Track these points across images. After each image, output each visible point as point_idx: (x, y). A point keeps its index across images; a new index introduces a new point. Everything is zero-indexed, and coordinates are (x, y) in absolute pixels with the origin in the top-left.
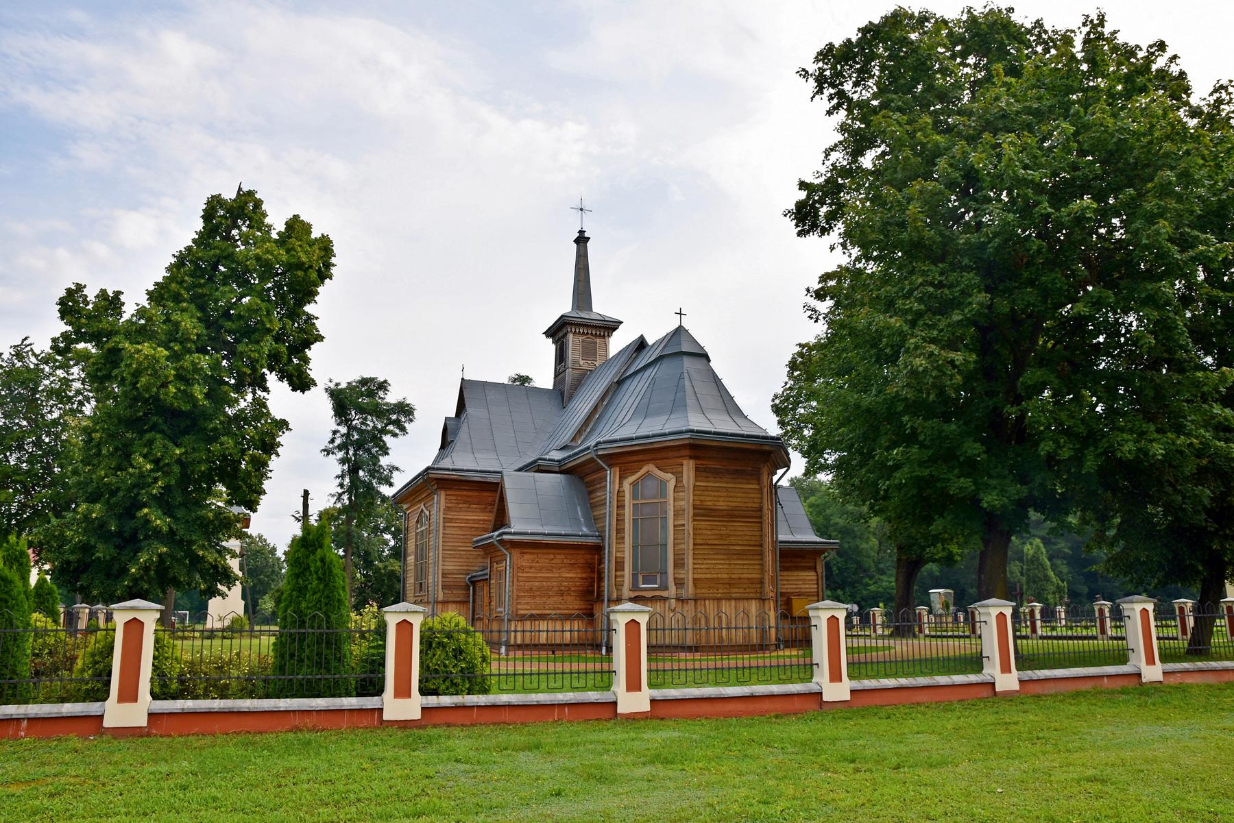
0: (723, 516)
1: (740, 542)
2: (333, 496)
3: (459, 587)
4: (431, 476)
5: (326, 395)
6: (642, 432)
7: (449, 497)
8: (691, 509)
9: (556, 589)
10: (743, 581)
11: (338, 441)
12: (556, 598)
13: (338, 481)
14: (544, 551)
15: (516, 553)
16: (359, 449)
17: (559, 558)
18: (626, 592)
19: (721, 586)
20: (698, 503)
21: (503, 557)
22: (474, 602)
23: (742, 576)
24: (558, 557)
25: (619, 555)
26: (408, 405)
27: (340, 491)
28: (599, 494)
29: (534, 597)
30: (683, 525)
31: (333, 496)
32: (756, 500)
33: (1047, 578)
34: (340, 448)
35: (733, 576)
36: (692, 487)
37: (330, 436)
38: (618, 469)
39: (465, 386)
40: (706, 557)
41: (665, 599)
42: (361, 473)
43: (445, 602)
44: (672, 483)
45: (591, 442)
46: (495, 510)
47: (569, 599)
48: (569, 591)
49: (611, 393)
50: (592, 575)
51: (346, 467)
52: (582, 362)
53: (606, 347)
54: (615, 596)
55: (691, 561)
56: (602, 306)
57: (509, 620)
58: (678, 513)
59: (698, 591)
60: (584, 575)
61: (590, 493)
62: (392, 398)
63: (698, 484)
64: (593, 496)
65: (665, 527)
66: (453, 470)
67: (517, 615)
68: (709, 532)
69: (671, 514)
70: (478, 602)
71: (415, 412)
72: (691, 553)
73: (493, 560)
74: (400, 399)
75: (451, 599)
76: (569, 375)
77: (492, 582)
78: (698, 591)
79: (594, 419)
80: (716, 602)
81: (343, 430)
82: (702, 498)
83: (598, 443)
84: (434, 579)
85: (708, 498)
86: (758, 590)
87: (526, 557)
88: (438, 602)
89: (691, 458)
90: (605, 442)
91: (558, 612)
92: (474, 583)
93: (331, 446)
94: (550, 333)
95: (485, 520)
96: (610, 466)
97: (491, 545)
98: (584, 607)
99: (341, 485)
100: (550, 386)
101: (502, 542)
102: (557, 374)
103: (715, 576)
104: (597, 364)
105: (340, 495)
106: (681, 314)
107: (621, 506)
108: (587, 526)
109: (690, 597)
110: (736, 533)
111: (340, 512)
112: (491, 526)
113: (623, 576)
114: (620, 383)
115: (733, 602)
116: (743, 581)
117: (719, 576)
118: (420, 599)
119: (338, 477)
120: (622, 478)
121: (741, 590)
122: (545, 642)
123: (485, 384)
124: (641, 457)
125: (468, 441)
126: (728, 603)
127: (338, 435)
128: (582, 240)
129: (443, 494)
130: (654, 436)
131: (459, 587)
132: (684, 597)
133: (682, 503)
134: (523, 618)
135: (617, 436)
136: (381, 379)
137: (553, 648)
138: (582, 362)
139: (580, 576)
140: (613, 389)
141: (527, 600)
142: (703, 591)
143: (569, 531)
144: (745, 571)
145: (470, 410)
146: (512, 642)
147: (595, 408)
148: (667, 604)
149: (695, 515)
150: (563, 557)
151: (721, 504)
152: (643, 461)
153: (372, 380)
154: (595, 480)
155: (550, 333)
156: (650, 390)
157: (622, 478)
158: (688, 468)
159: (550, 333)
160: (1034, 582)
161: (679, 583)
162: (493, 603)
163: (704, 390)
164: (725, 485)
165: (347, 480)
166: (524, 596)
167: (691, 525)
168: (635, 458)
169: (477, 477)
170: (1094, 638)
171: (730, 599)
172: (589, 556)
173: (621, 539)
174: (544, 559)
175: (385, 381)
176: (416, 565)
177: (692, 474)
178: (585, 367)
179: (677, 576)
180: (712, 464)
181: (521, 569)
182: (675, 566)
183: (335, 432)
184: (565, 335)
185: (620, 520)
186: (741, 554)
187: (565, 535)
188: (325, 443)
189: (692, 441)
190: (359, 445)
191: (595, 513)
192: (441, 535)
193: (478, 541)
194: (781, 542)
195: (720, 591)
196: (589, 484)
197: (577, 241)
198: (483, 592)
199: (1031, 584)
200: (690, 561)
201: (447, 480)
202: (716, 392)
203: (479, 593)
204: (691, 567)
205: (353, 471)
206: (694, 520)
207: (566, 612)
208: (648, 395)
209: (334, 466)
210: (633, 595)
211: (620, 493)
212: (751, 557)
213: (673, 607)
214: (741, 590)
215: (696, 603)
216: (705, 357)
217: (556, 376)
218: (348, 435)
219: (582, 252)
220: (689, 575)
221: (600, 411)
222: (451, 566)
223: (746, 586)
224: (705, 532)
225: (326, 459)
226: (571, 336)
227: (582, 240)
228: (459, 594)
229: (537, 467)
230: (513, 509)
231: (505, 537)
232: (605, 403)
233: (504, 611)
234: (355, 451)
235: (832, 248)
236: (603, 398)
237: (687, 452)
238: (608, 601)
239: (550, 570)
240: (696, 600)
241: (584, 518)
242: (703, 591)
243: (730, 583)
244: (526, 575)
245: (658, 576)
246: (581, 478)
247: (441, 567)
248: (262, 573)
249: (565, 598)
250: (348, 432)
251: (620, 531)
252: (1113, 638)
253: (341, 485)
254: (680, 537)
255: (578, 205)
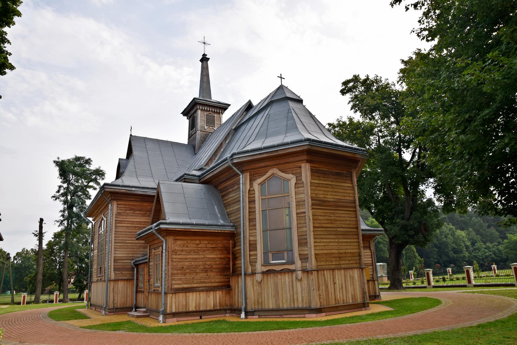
0: (331, 206)
1: (344, 226)
2: (58, 222)
3: (127, 269)
4: (106, 190)
5: (54, 164)
6: (265, 145)
7: (119, 206)
8: (310, 200)
9: (202, 267)
10: (348, 255)
11: (62, 191)
12: (202, 275)
13: (61, 214)
14: (193, 238)
15: (170, 239)
16: (73, 196)
17: (204, 243)
18: (259, 268)
19: (333, 259)
20: (314, 195)
21: (160, 244)
22: (137, 279)
23: (347, 251)
24: (202, 242)
25: (252, 238)
26: (101, 171)
27: (62, 218)
28: (231, 195)
29: (185, 274)
30: (304, 213)
31: (58, 222)
32: (351, 195)
33: (415, 257)
34: (63, 195)
35: (341, 251)
36: (309, 183)
37: (57, 189)
38: (248, 174)
39: (132, 139)
40: (323, 237)
41: (292, 271)
42: (74, 209)
43: (116, 280)
44: (293, 181)
45: (228, 155)
46: (152, 215)
47: (212, 274)
48: (211, 269)
49: (230, 136)
50: (228, 256)
51: (66, 206)
52: (206, 127)
53: (220, 119)
54: (250, 271)
55: (312, 240)
56: (216, 96)
57: (166, 293)
58: (300, 204)
59: (319, 264)
60: (222, 256)
61: (223, 196)
62: (93, 167)
63: (313, 181)
64: (226, 198)
65: (289, 215)
66: (123, 186)
67: (172, 289)
68: (323, 218)
69: (294, 204)
70: (140, 278)
71: (106, 175)
72: (312, 234)
73: (152, 247)
74: (97, 167)
75: (121, 278)
76: (199, 135)
77: (151, 264)
78: (319, 264)
79: (220, 152)
80: (331, 271)
81: (65, 185)
82: (317, 192)
83: (234, 154)
84: (110, 265)
85: (320, 192)
86: (358, 262)
87: (178, 242)
88: (110, 280)
89: (308, 161)
90: (239, 153)
91: (204, 285)
92: (137, 266)
93: (58, 194)
94: (185, 112)
95: (145, 222)
96: (243, 172)
97: (152, 234)
98: (223, 280)
99: (63, 216)
100: (186, 142)
101: (160, 231)
102: (190, 137)
103: (329, 251)
104: (215, 129)
105: (62, 221)
106: (281, 78)
107: (252, 201)
108: (224, 220)
109: (314, 268)
110: (340, 219)
111: (62, 231)
112: (150, 220)
113: (256, 255)
114: (237, 129)
115: (343, 271)
116: (348, 255)
117: (332, 251)
118: (99, 278)
119: (61, 211)
120: (252, 181)
121: (347, 262)
122: (194, 310)
123: (145, 139)
124: (267, 163)
125: (134, 170)
126: (339, 272)
127: (62, 188)
128: (204, 59)
129: (115, 204)
130: (278, 146)
131: (127, 269)
132: (309, 268)
133: (302, 196)
134: (177, 291)
135: (249, 148)
136: (87, 158)
137: (200, 313)
138: (206, 127)
139: (219, 256)
140: (232, 133)
141: (180, 277)
142: (322, 263)
143: (211, 222)
144: (348, 247)
145: (135, 152)
146: (168, 311)
147: (221, 145)
148: (294, 275)
149: (313, 204)
150: (206, 242)
151: (329, 196)
152: (267, 166)
153: (82, 158)
154: (227, 186)
155: (185, 113)
156: (266, 122)
157: (252, 181)
158: (306, 169)
159: (185, 113)
160: (410, 259)
161: (304, 258)
162: (152, 280)
163: (306, 120)
164: (330, 183)
165: (66, 212)
166: (178, 274)
167: (311, 212)
168: (262, 164)
169: (140, 192)
170: (465, 286)
171: (340, 269)
172: (226, 242)
173: (253, 226)
174: (192, 244)
175: (89, 159)
176: (98, 255)
177: (309, 174)
178: (208, 130)
179: (301, 252)
180: (323, 168)
181: (175, 252)
182: (300, 244)
183: (60, 187)
184: (196, 111)
185: (252, 212)
186: (345, 235)
187: (208, 225)
188: (54, 192)
189: (310, 147)
190: (74, 194)
191: (228, 210)
192: (114, 232)
193: (140, 234)
194: (362, 230)
195: (333, 263)
196: (221, 191)
197: (202, 60)
198: (143, 271)
199: (408, 260)
200: (311, 240)
201: (118, 193)
202: (313, 123)
203: (141, 272)
204: (313, 244)
205: (70, 207)
206: (313, 209)
207: (210, 285)
208: (264, 128)
209: (60, 205)
210: (265, 269)
211: (251, 192)
212: (351, 237)
213: (299, 278)
214: (347, 262)
215: (318, 273)
216: (300, 101)
217: (189, 138)
218: (68, 188)
219: (205, 66)
220: (311, 251)
221: (224, 146)
222: (121, 254)
223: (350, 258)
224: (320, 218)
225: (55, 202)
226: (199, 112)
227: (204, 59)
228: (126, 274)
229: (184, 179)
230: (167, 207)
231: (162, 226)
232: (227, 142)
233: (161, 285)
234: (71, 197)
235: (407, 9)
236: (225, 139)
237: (305, 157)
238: (245, 275)
239: (197, 252)
240: (317, 271)
241: (220, 213)
242: (322, 263)
243: (340, 257)
244: (178, 257)
245: (285, 254)
246: (216, 187)
247: (113, 255)
248: (31, 268)
249: (209, 274)
250: (68, 186)
251: (252, 220)
252: (475, 286)
253: (63, 216)
254: (302, 222)
255: (202, 40)
